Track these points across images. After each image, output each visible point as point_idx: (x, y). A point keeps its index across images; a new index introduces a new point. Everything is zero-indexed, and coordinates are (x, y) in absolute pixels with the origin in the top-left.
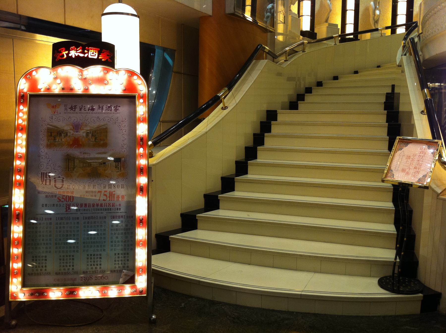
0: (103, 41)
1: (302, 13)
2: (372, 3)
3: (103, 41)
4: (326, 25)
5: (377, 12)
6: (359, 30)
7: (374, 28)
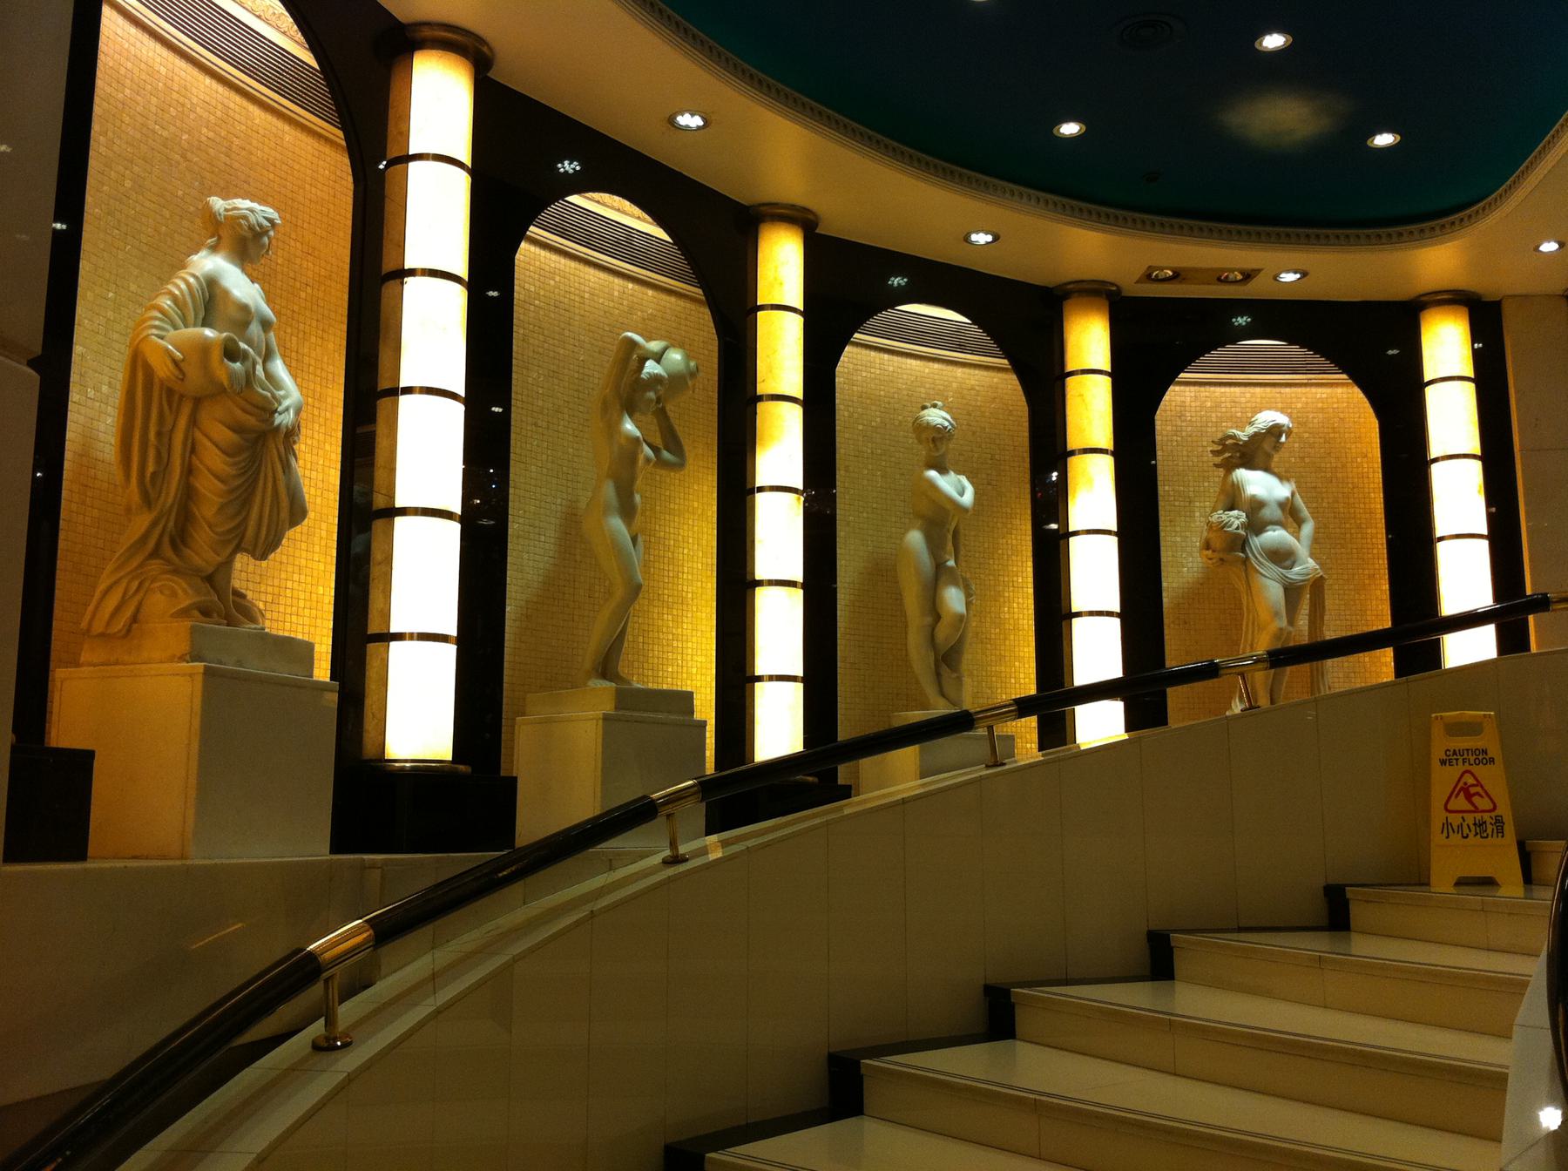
0: (1120, 675)
1: (386, 616)
2: (915, 538)
3: (1120, 675)
4: (599, 698)
5: (953, 598)
6: (844, 733)
7: (941, 709)
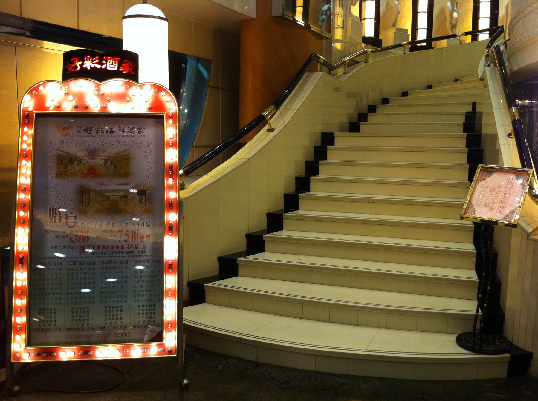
1: (365, 16)
2: (449, 4)
4: (394, 30)
5: (455, 15)
6: (434, 36)
7: (451, 34)
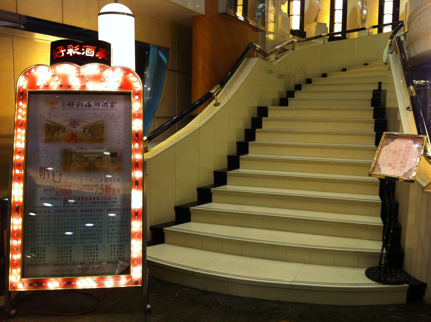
2: (360, 3)
4: (315, 24)
5: (365, 12)
6: (347, 29)
7: (361, 27)
